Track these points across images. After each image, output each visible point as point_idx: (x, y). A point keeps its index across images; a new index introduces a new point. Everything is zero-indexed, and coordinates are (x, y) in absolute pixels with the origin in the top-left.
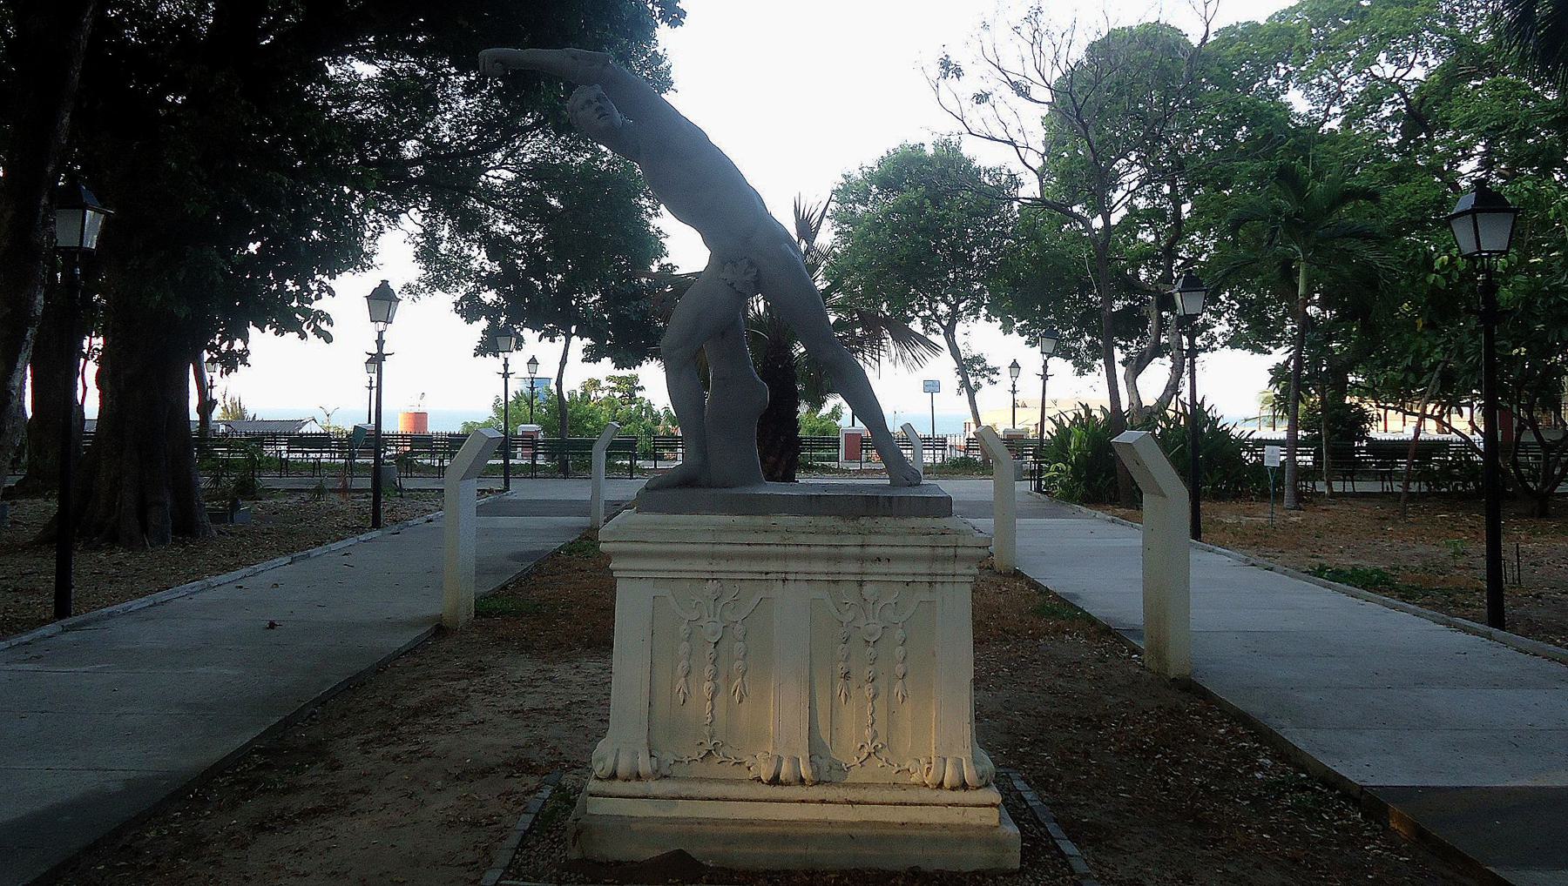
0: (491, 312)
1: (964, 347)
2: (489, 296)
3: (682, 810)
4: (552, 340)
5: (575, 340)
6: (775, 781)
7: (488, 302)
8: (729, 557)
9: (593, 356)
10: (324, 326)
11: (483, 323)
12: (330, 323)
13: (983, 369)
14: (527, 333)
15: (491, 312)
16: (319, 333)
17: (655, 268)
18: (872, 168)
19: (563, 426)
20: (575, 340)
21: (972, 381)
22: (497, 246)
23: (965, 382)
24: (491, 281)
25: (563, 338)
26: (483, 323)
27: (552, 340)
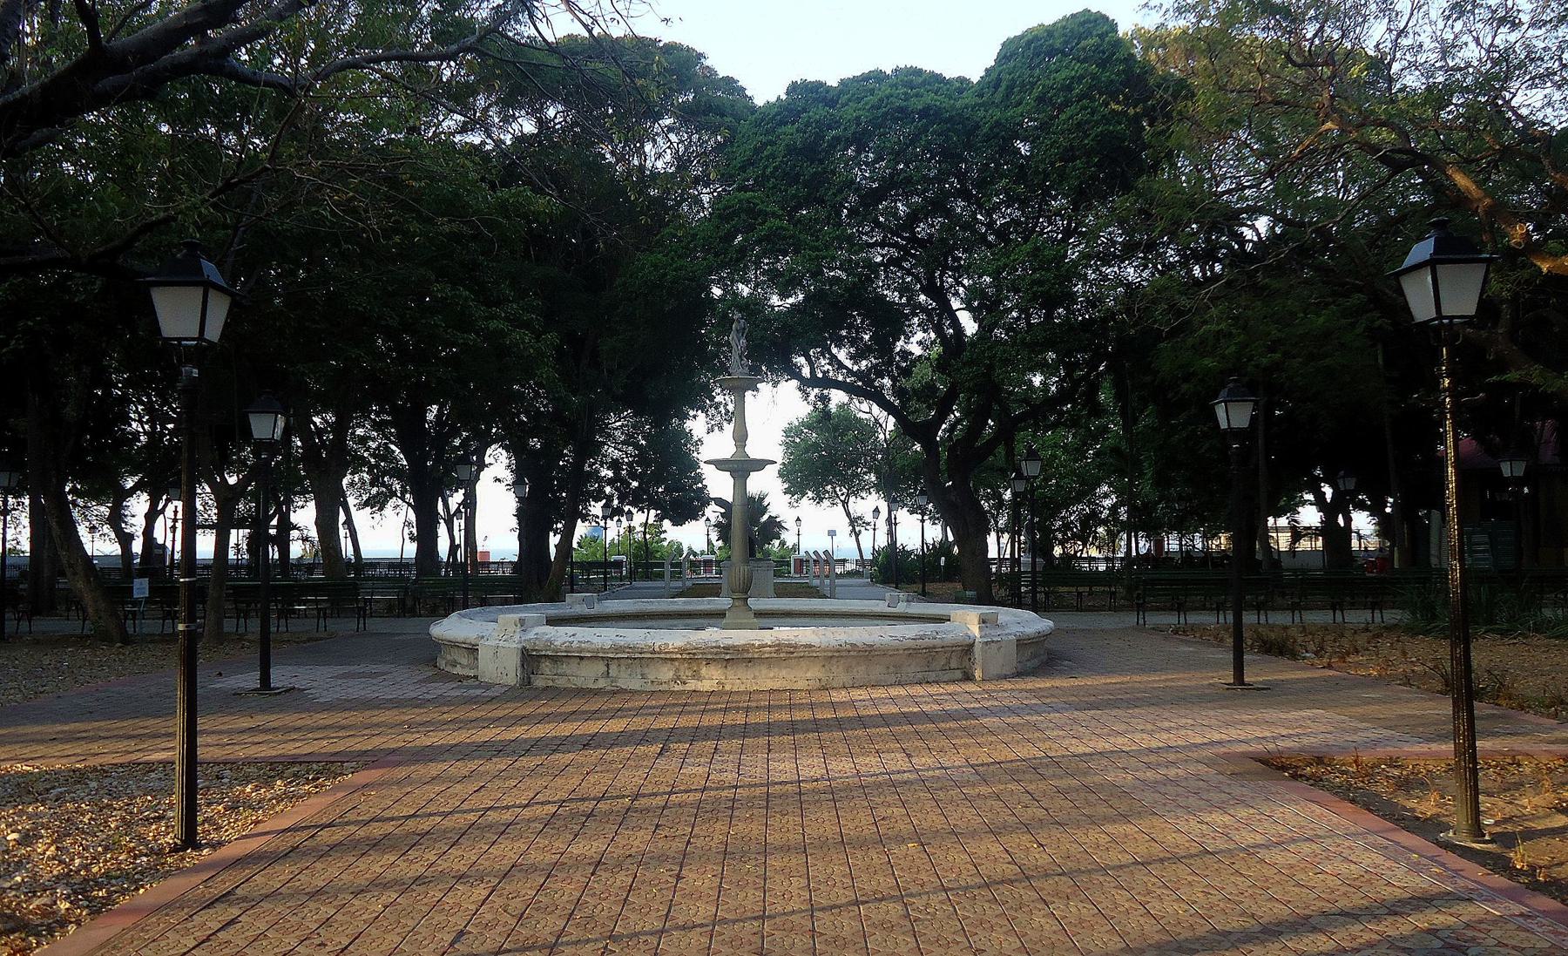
21: (857, 529)
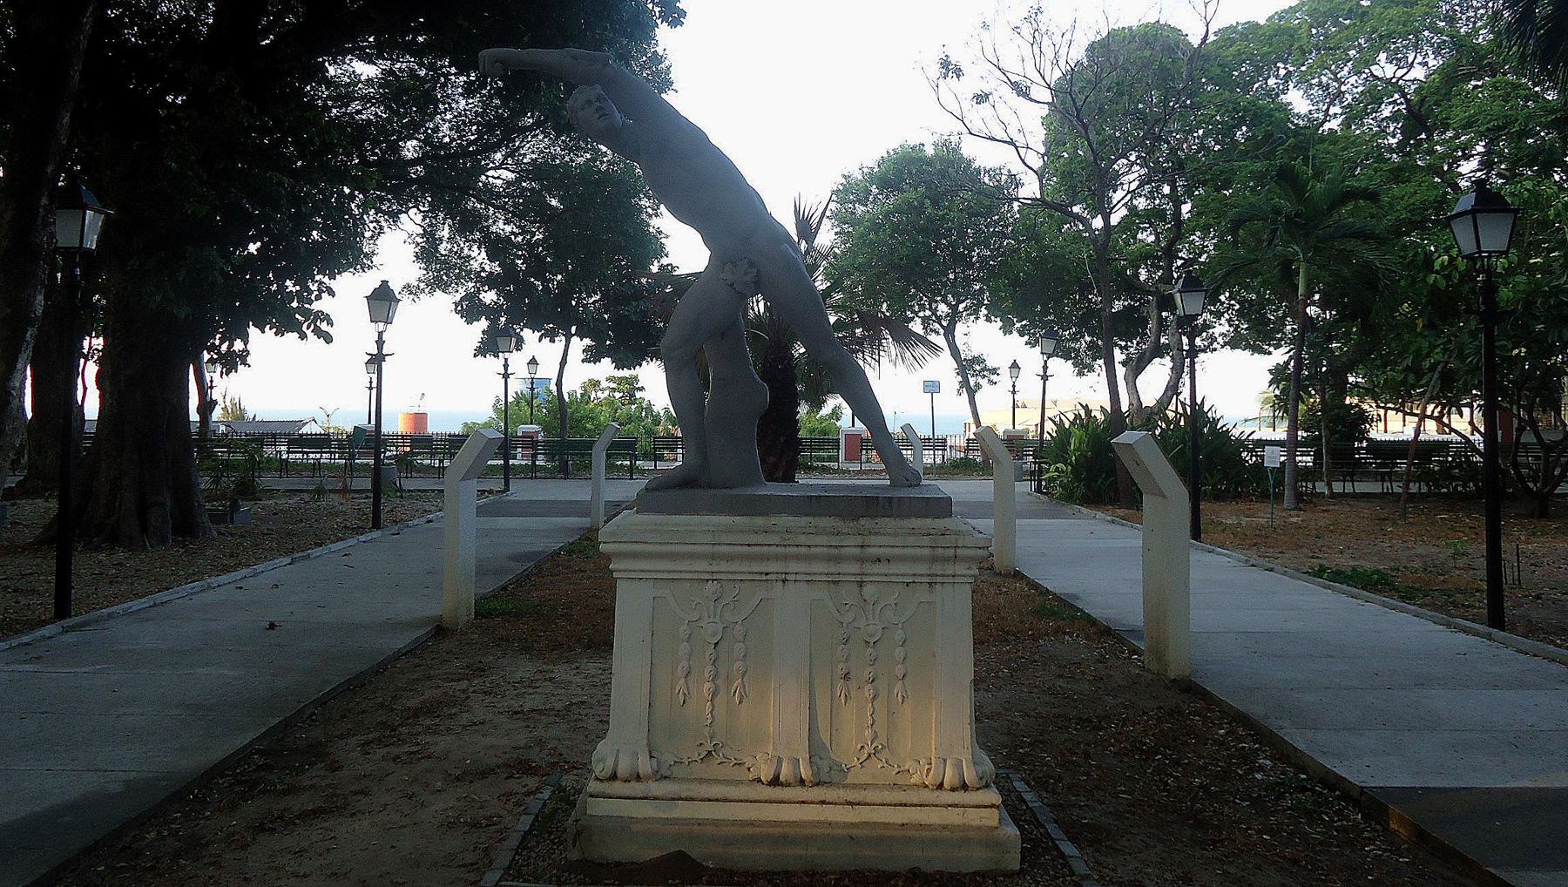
0: (491, 312)
1: (964, 348)
2: (489, 297)
3: (682, 811)
4: (552, 341)
5: (575, 340)
6: (775, 782)
7: (488, 302)
8: (729, 558)
9: (593, 356)
10: (324, 326)
11: (483, 324)
12: (330, 323)
13: (983, 370)
14: (527, 334)
15: (491, 312)
16: (319, 333)
17: (655, 269)
18: (872, 169)
19: (563, 426)
20: (575, 340)
21: (972, 381)
22: (497, 247)
23: (965, 383)
24: (491, 281)
25: (563, 338)
26: (483, 324)
27: (552, 341)
